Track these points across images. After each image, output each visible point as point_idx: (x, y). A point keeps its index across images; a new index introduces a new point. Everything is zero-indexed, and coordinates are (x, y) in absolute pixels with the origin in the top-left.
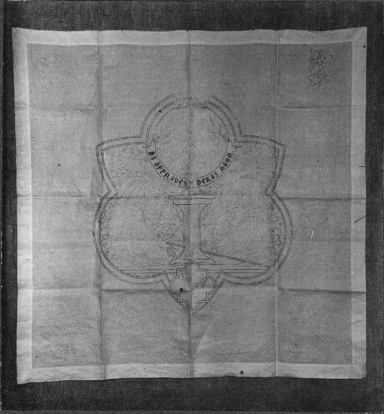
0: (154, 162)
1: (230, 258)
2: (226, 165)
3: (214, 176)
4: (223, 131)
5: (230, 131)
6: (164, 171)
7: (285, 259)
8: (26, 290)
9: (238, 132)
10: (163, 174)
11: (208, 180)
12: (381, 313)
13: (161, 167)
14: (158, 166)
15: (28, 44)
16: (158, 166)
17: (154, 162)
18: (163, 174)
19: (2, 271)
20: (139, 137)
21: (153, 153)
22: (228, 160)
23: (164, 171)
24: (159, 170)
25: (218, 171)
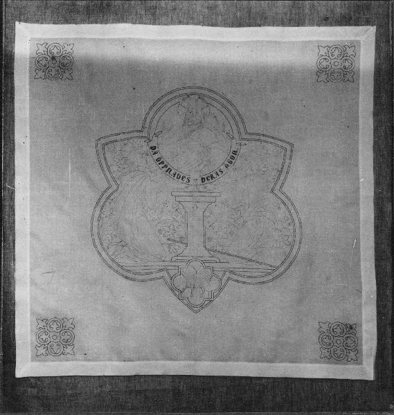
0: (156, 156)
1: (237, 256)
2: (231, 162)
3: (219, 173)
4: (228, 128)
5: (234, 127)
6: (163, 162)
7: (295, 257)
8: (41, 312)
9: (242, 130)
10: (165, 169)
11: (212, 177)
12: (391, 299)
13: (163, 162)
14: (159, 161)
15: (358, 42)
16: (159, 161)
17: (156, 156)
18: (165, 169)
19: (4, 336)
20: (140, 131)
21: (155, 147)
22: (233, 158)
23: (166, 166)
24: (161, 166)
25: (223, 168)
